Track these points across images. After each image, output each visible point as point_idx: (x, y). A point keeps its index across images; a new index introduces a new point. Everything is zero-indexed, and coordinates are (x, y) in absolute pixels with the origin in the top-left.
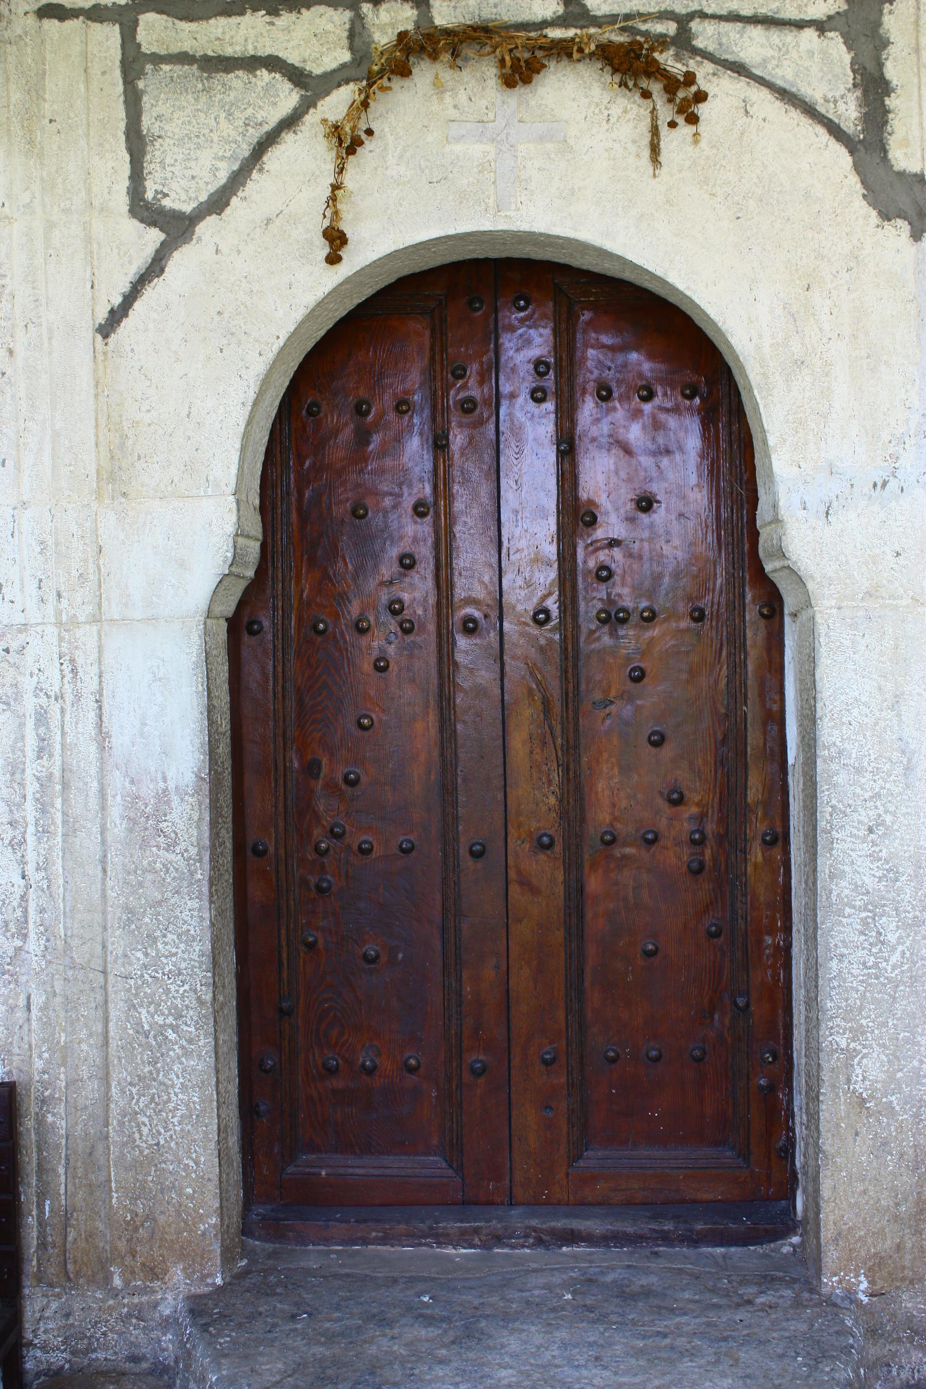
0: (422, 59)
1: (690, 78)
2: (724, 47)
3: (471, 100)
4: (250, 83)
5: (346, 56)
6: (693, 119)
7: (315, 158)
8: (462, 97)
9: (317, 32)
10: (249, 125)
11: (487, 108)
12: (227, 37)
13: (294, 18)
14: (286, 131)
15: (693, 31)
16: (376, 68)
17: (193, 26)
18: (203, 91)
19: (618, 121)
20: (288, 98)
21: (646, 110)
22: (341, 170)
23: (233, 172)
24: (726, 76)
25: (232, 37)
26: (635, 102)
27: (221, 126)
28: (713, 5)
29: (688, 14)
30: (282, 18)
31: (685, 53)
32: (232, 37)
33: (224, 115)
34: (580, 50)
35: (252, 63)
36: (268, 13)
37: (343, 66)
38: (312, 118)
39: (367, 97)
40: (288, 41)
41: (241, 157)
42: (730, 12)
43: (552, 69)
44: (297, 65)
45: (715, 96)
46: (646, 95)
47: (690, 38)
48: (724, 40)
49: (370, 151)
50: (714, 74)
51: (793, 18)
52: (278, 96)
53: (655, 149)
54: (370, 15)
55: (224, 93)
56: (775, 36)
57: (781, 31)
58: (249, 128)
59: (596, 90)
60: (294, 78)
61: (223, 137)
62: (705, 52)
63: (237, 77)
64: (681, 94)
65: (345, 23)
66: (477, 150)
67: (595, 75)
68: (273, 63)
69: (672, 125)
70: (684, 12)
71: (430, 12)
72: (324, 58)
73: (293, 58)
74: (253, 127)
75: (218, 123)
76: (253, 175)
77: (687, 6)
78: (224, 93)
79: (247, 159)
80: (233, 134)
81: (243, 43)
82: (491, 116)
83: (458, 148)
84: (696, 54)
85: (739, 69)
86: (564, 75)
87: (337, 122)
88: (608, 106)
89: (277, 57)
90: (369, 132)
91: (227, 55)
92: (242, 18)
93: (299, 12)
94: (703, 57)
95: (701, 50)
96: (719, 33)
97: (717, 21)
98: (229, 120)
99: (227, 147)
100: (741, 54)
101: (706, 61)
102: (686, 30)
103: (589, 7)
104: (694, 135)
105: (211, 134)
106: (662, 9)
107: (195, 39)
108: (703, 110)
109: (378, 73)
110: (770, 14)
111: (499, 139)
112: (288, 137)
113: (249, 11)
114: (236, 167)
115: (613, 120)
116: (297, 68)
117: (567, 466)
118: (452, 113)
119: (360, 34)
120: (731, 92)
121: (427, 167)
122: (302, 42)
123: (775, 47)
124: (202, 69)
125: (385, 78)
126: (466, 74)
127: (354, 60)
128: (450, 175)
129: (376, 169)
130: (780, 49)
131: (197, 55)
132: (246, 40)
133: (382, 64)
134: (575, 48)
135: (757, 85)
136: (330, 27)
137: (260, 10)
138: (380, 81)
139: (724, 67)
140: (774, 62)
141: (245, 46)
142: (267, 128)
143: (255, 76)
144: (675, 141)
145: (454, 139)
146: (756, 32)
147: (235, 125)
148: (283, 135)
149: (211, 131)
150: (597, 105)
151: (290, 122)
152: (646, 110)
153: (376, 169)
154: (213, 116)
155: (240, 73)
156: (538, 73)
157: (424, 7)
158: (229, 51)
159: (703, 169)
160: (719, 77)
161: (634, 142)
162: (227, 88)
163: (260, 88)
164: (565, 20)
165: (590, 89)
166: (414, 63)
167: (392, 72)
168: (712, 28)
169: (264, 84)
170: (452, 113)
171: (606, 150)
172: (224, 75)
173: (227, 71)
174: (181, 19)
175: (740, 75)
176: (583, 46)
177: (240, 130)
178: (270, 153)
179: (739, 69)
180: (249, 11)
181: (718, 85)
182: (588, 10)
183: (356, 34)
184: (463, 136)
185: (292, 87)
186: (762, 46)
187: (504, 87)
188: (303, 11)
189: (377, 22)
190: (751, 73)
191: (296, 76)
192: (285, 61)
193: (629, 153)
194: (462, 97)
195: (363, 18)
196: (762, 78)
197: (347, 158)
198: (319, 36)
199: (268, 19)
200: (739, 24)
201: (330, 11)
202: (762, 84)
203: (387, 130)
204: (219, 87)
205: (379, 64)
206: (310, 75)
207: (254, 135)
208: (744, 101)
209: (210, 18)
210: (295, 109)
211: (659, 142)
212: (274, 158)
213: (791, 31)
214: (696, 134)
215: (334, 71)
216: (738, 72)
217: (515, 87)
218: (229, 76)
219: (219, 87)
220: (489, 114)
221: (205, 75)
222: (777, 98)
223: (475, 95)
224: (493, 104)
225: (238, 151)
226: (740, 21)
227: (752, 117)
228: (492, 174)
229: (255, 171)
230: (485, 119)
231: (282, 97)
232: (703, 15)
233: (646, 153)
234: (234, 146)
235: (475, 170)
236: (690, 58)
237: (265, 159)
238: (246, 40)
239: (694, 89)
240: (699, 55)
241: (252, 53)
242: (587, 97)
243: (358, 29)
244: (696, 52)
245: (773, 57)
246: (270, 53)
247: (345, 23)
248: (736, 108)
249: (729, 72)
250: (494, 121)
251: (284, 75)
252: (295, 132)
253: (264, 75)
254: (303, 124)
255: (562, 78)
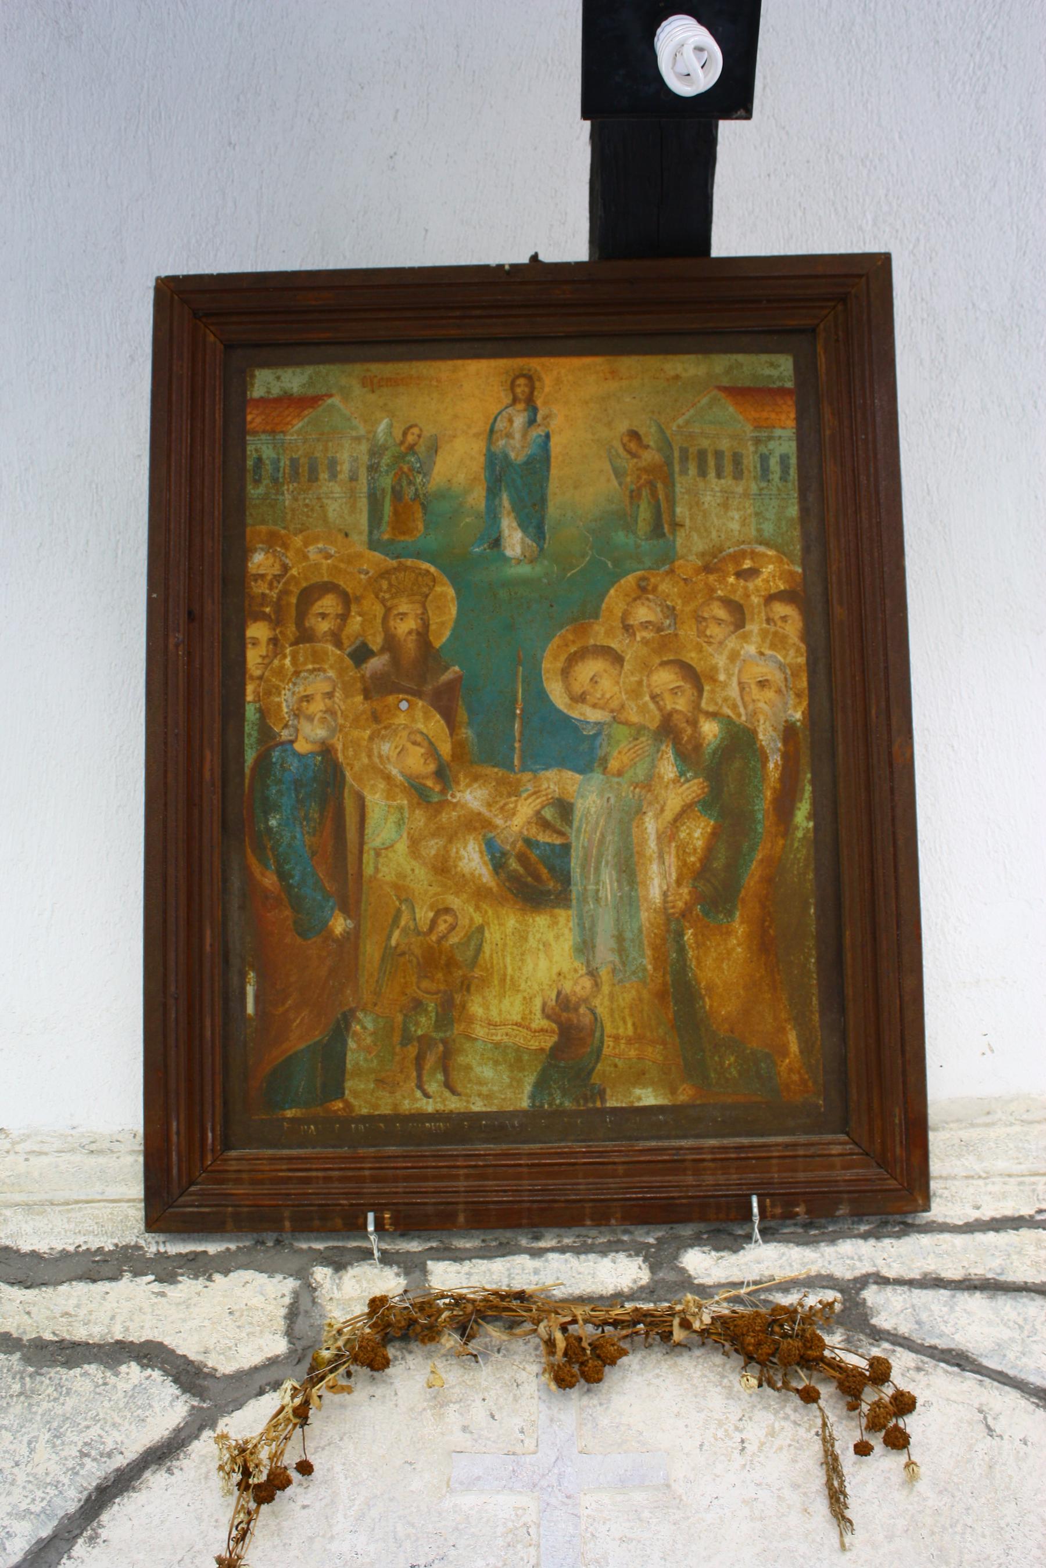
0: (410, 1352)
1: (880, 1372)
2: (927, 1327)
3: (493, 1417)
4: (105, 1384)
5: (279, 1346)
6: (898, 1441)
7: (199, 1519)
8: (478, 1413)
9: (234, 1308)
10: (87, 1455)
11: (522, 1432)
12: (82, 1312)
13: (200, 1287)
14: (154, 1467)
15: (869, 1303)
16: (326, 1354)
17: (31, 1294)
18: (21, 1394)
19: (760, 1450)
20: (167, 1408)
21: (808, 1430)
22: (242, 1535)
23: (40, 1541)
24: (940, 1371)
25: (90, 1312)
26: (786, 1418)
27: (36, 1457)
28: (894, 1265)
29: (855, 1280)
30: (180, 1286)
31: (862, 1337)
32: (90, 1312)
33: (48, 1436)
34: (686, 1325)
35: (116, 1353)
36: (159, 1280)
37: (273, 1362)
38: (204, 1449)
39: (306, 1403)
40: (184, 1320)
41: (61, 1513)
42: (926, 1275)
43: (635, 1366)
44: (192, 1357)
45: (927, 1404)
46: (809, 1396)
47: (866, 1315)
48: (924, 1316)
49: (304, 1507)
50: (918, 1369)
51: (1030, 1280)
52: (151, 1406)
53: (837, 1498)
54: (327, 1284)
55: (55, 1400)
56: (1008, 1308)
57: (1015, 1299)
58: (86, 1460)
59: (716, 1400)
60: (183, 1378)
61: (35, 1476)
62: (896, 1335)
63: (86, 1374)
64: (870, 1396)
65: (283, 1296)
66: (505, 1505)
67: (711, 1376)
68: (151, 1354)
69: (863, 1449)
70: (849, 1276)
71: (427, 1280)
72: (241, 1349)
73: (187, 1346)
74: (94, 1460)
75: (32, 1451)
76: (77, 1547)
77: (853, 1268)
78: (55, 1400)
79: (70, 1518)
80: (55, 1469)
81: (107, 1321)
82: (530, 1443)
83: (467, 1501)
84: (881, 1339)
85: (960, 1360)
86: (658, 1376)
87: (246, 1442)
88: (740, 1425)
89: (161, 1344)
90: (305, 1468)
91: (76, 1339)
92: (114, 1284)
93: (210, 1279)
94: (893, 1343)
95: (888, 1332)
96: (913, 1306)
97: (905, 1288)
98: (54, 1446)
99: (39, 1494)
100: (957, 1337)
101: (899, 1349)
102: (857, 1304)
103: (692, 1272)
104: (907, 1466)
105: (16, 1470)
106: (813, 1273)
107: (28, 1313)
108: (911, 1423)
109: (330, 1362)
110: (990, 1276)
111: (544, 1483)
112: (156, 1480)
113: (127, 1275)
114: (45, 1533)
115: (751, 1448)
116: (192, 1362)
117: (836, 1484)
118: (459, 1439)
119: (306, 1312)
120: (953, 1397)
121: (408, 1536)
122: (207, 1323)
123: (1011, 1324)
124: (27, 1360)
125: (342, 1370)
126: (485, 1374)
127: (292, 1352)
128: (453, 1552)
129: (311, 1539)
130: (1021, 1327)
131: (25, 1338)
132: (113, 1318)
133: (339, 1349)
134: (676, 1322)
135: (996, 1384)
136: (257, 1301)
137: (146, 1275)
138: (331, 1376)
139: (932, 1357)
140: (1017, 1348)
141: (108, 1326)
142: (120, 1461)
143: (117, 1374)
144: (871, 1478)
145: (461, 1483)
146: (976, 1302)
147: (63, 1454)
148: (147, 1474)
149: (17, 1464)
150: (720, 1423)
151: (163, 1454)
152: (808, 1430)
153: (311, 1539)
154: (26, 1439)
155: (92, 1368)
156: (613, 1363)
157: (417, 1274)
158: (80, 1334)
159: (933, 1533)
160: (927, 1373)
161: (796, 1486)
162: (63, 1391)
163: (121, 1394)
164: (652, 1292)
165: (704, 1397)
166: (396, 1358)
167: (355, 1359)
168: (901, 1299)
169: (128, 1387)
170: (459, 1439)
171: (745, 1502)
172: (63, 1371)
173: (69, 1364)
174: (12, 1284)
175: (963, 1370)
176: (689, 1317)
177: (70, 1464)
178: (116, 1507)
179: (960, 1360)
180: (127, 1275)
181: (928, 1385)
182: (690, 1276)
183: (297, 1313)
184: (478, 1478)
185: (178, 1392)
186: (990, 1323)
187: (553, 1386)
188: (217, 1277)
189: (337, 1295)
190: (980, 1365)
191: (188, 1375)
192: (173, 1351)
193: (789, 1507)
194: (478, 1413)
195: (315, 1289)
196: (1001, 1373)
197: (257, 1511)
198: (237, 1314)
199: (157, 1287)
200: (942, 1291)
201: (261, 1278)
202: (1004, 1384)
203: (338, 1468)
204: (50, 1390)
205: (333, 1348)
206: (212, 1375)
207: (94, 1473)
208: (980, 1411)
209: (62, 1282)
210: (178, 1430)
211: (842, 1483)
212: (120, 1519)
213: (1033, 1300)
214: (910, 1464)
215: (256, 1369)
216: (958, 1365)
217: (571, 1386)
218: (72, 1372)
219: (50, 1390)
220: (526, 1442)
221: (31, 1369)
222: (1038, 1406)
223: (501, 1408)
224: (533, 1423)
225: (58, 1501)
226: (945, 1288)
227: (1001, 1437)
228: (532, 1550)
229: (80, 1541)
230: (518, 1449)
231: (157, 1409)
232: (883, 1281)
233: (821, 1506)
234: (52, 1491)
235: (500, 1542)
236: (871, 1344)
237: (105, 1517)
238: (113, 1318)
239: (888, 1391)
240: (887, 1340)
241: (119, 1337)
242: (700, 1411)
243: (305, 1303)
244: (878, 1335)
245: (1012, 1340)
246: (150, 1338)
247: (283, 1296)
248: (969, 1423)
249: (942, 1365)
250: (535, 1453)
251: (166, 1373)
252: (169, 1471)
253: (132, 1371)
254: (187, 1456)
255: (655, 1381)
